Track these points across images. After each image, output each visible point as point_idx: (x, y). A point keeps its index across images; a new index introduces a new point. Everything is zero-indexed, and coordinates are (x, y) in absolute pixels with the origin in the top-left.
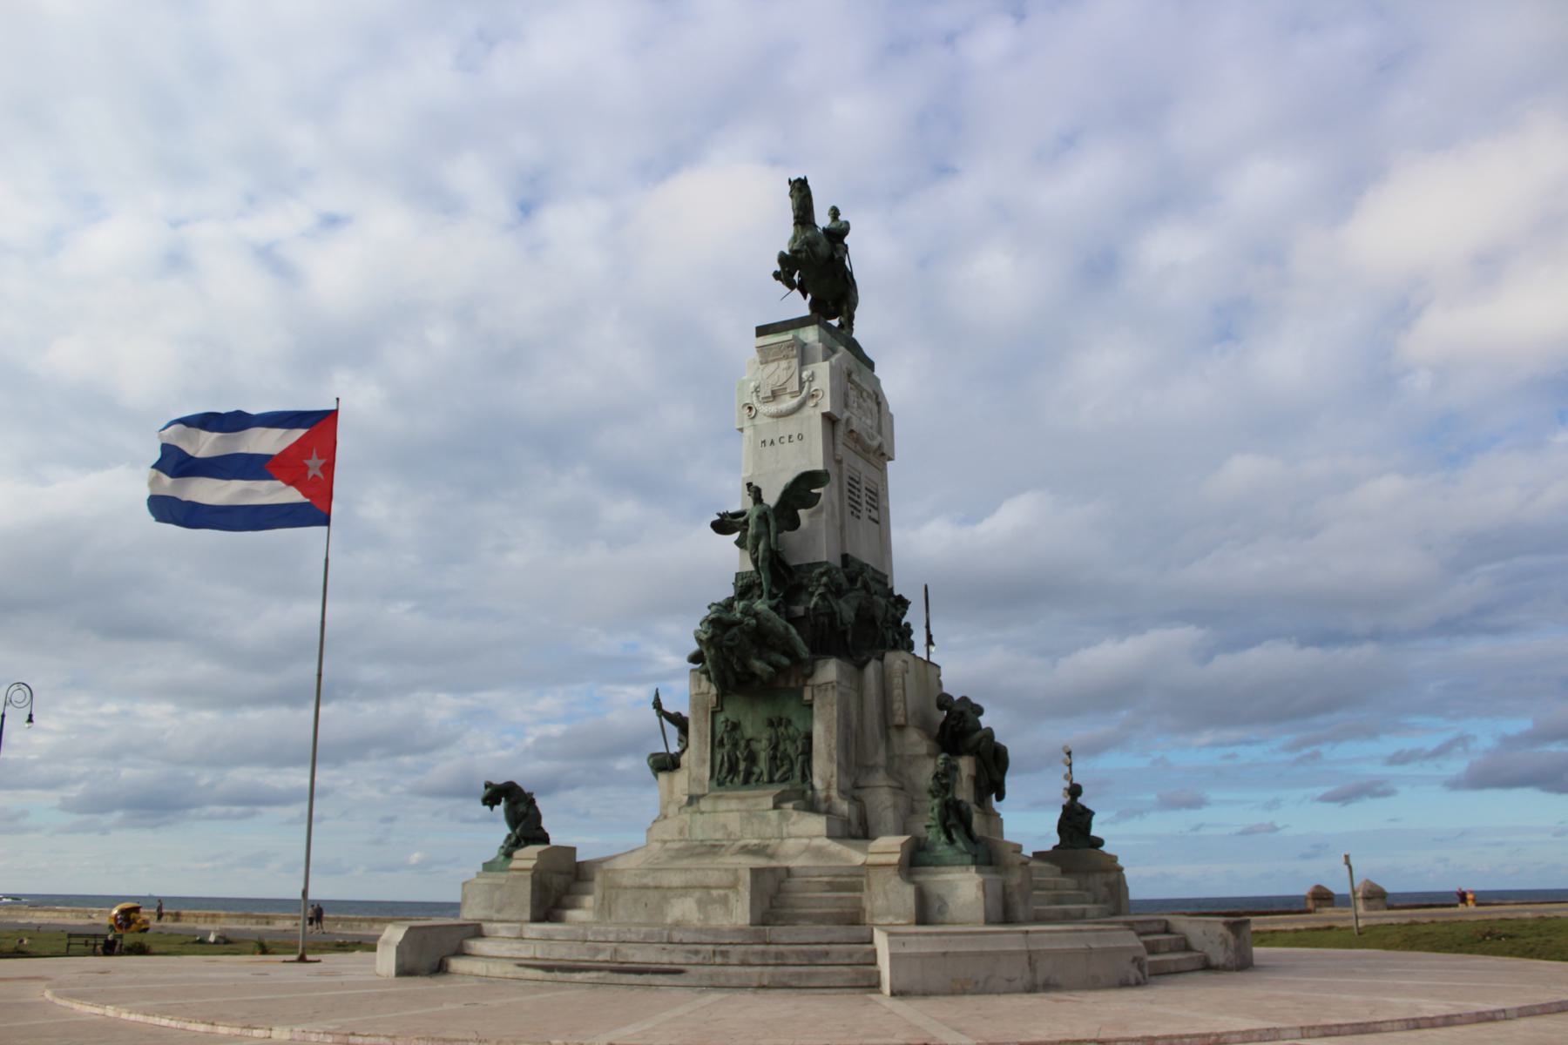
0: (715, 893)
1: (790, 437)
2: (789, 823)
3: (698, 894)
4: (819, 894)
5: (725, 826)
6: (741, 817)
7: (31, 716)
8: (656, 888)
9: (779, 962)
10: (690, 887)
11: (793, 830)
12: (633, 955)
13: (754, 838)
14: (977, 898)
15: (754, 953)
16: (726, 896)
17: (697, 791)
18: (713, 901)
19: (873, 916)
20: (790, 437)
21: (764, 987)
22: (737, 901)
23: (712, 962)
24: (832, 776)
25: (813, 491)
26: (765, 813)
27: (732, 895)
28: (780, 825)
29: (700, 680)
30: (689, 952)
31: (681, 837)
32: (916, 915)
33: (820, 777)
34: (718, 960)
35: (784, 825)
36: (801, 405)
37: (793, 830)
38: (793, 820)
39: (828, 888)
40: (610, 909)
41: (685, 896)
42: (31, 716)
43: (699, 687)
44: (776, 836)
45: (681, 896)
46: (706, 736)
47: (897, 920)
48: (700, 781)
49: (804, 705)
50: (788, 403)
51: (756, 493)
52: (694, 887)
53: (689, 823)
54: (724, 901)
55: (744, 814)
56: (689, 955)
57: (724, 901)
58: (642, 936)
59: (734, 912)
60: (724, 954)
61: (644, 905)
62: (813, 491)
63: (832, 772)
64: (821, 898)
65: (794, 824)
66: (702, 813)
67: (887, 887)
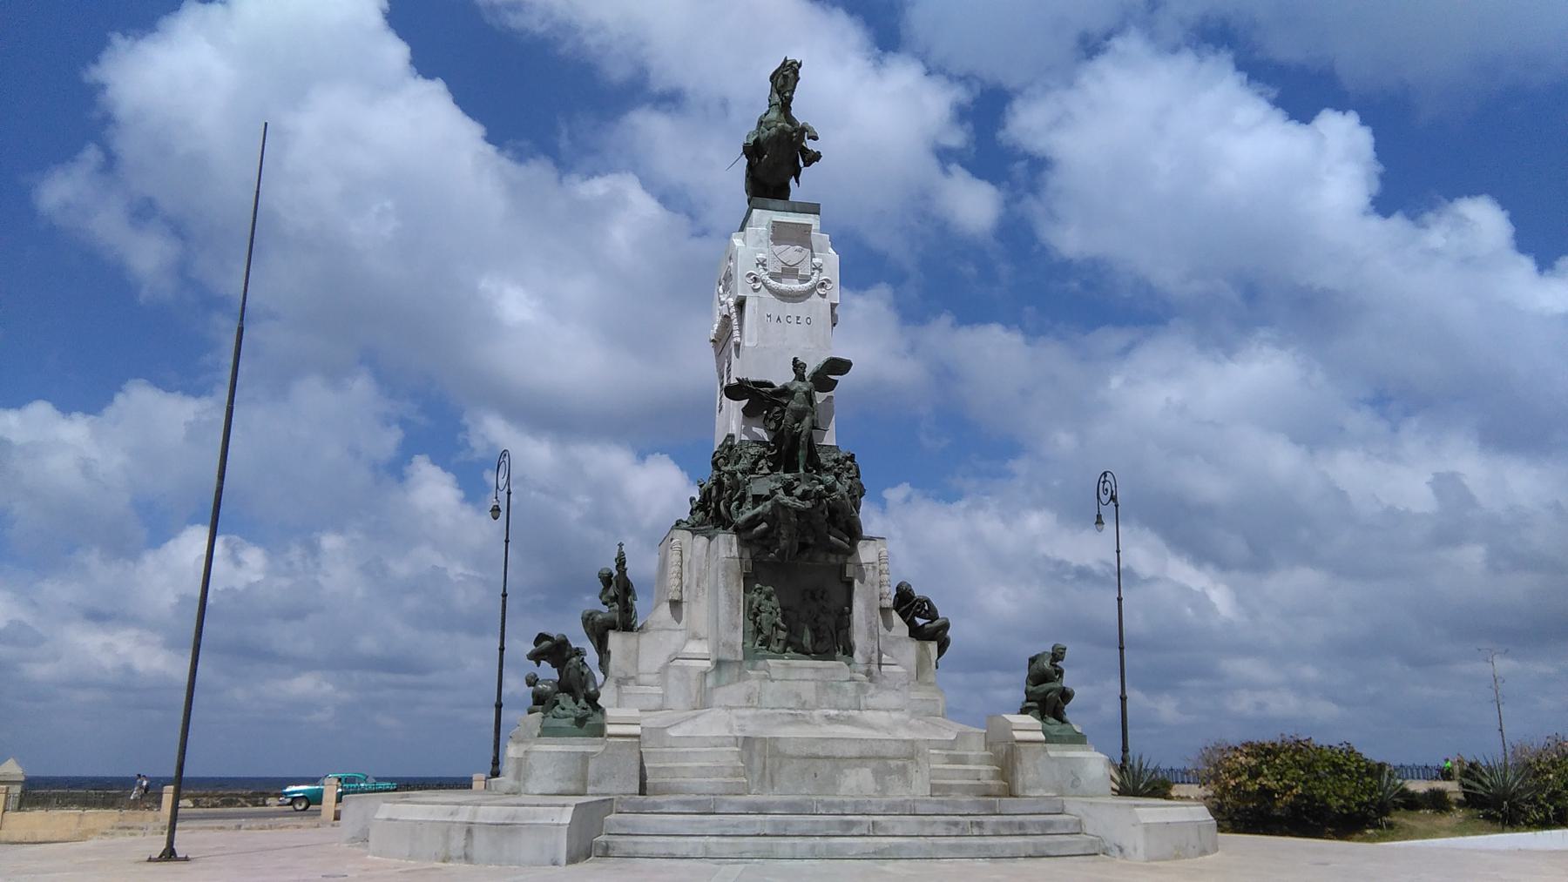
0: (893, 763)
1: (798, 318)
2: (867, 695)
3: (874, 764)
4: (941, 766)
5: (798, 695)
6: (817, 687)
7: (1099, 516)
8: (827, 758)
9: (1022, 832)
10: (865, 758)
11: (871, 702)
12: (893, 828)
13: (830, 708)
14: (1105, 774)
15: (1004, 824)
16: (904, 767)
17: (726, 655)
18: (890, 772)
19: (1024, 788)
20: (798, 318)
21: (1030, 857)
22: (917, 771)
23: (970, 834)
24: (873, 652)
25: (829, 376)
26: (842, 684)
27: (908, 763)
28: (857, 697)
29: (731, 544)
30: (948, 823)
31: (750, 705)
32: (61, 777)
33: (861, 652)
34: (976, 831)
35: (862, 697)
36: (812, 290)
37: (871, 702)
38: (870, 692)
39: (947, 761)
40: (772, 781)
41: (860, 767)
42: (1099, 516)
43: (731, 551)
44: (853, 706)
45: (856, 766)
46: (739, 601)
47: (1047, 792)
48: (730, 646)
49: (842, 582)
50: (795, 285)
51: (798, 366)
52: (870, 758)
53: (758, 690)
54: (903, 771)
55: (819, 683)
56: (949, 827)
57: (903, 771)
58: (883, 808)
59: (914, 783)
60: (980, 825)
61: (813, 775)
62: (829, 376)
63: (873, 648)
64: (944, 769)
65: (872, 696)
66: (772, 681)
67: (1038, 762)
